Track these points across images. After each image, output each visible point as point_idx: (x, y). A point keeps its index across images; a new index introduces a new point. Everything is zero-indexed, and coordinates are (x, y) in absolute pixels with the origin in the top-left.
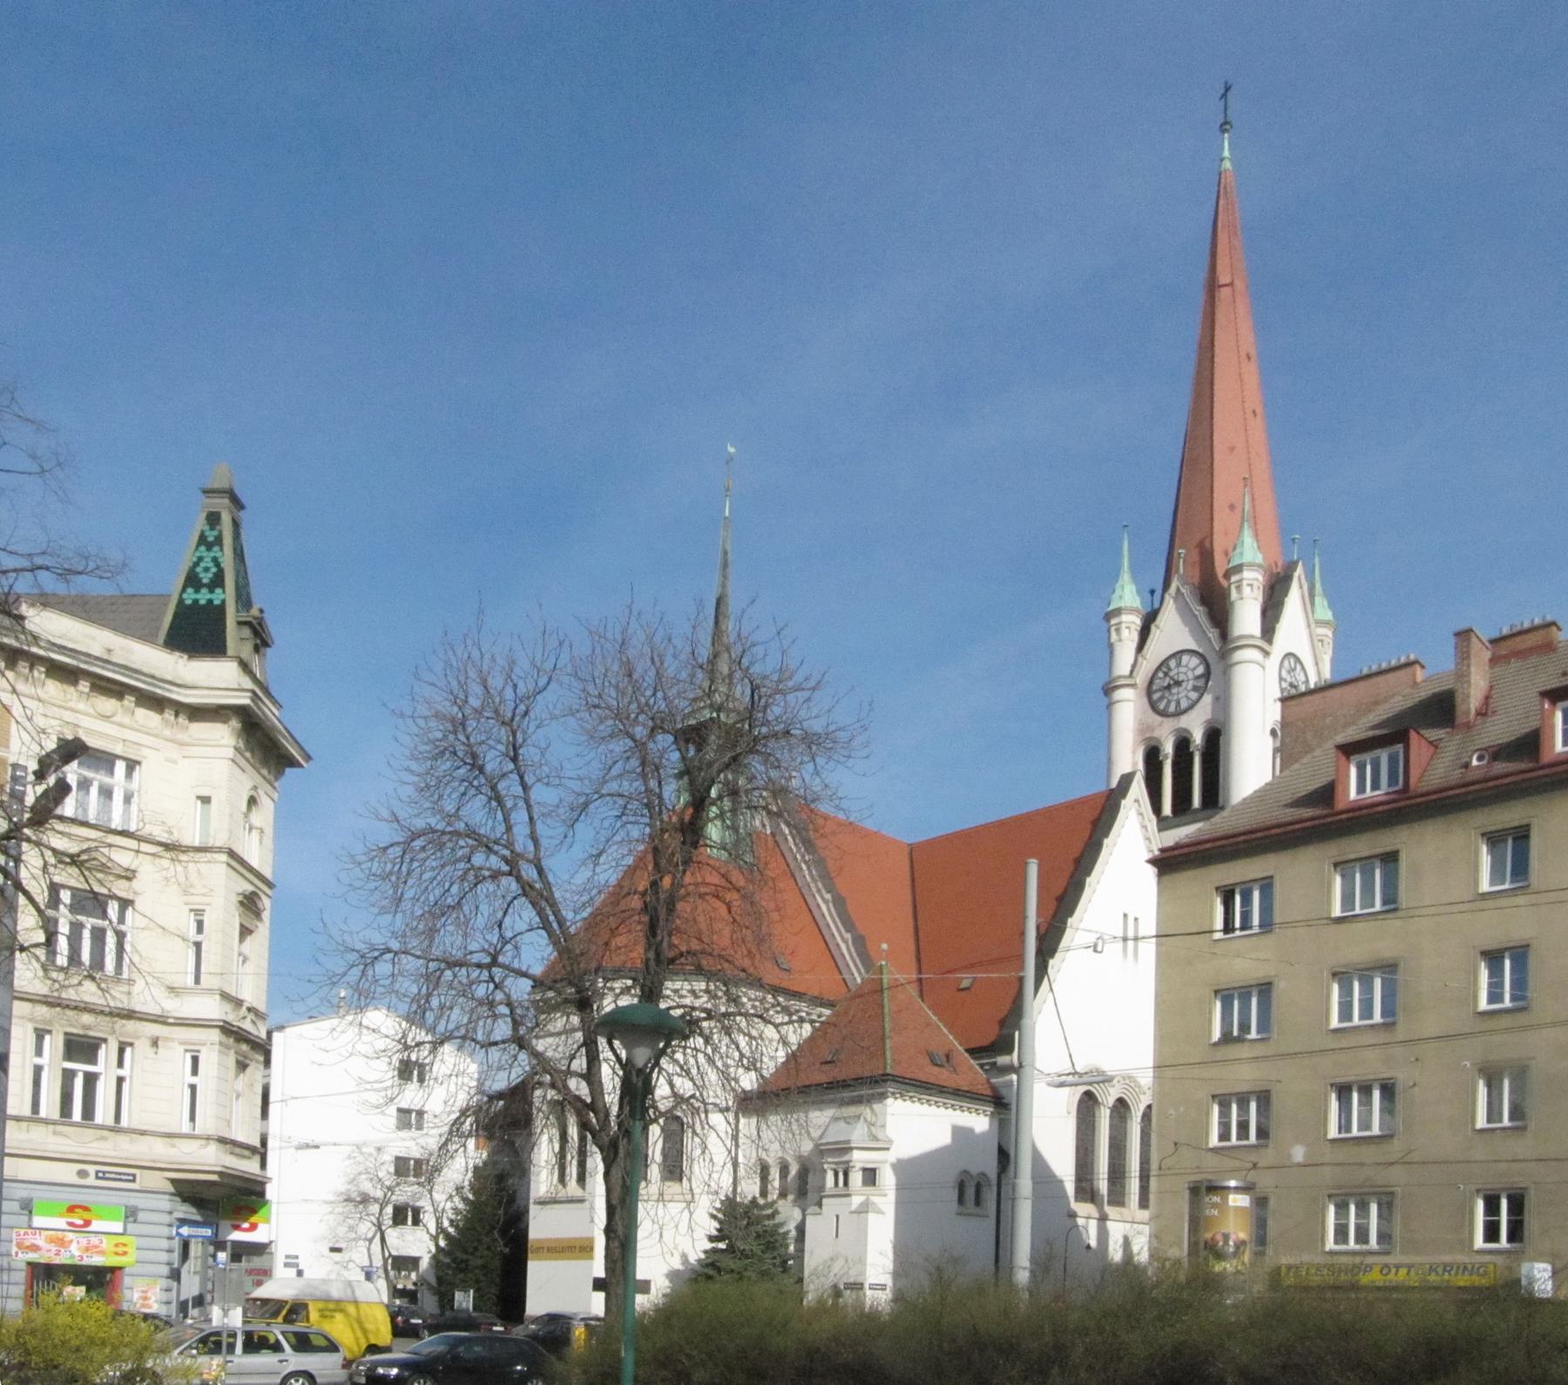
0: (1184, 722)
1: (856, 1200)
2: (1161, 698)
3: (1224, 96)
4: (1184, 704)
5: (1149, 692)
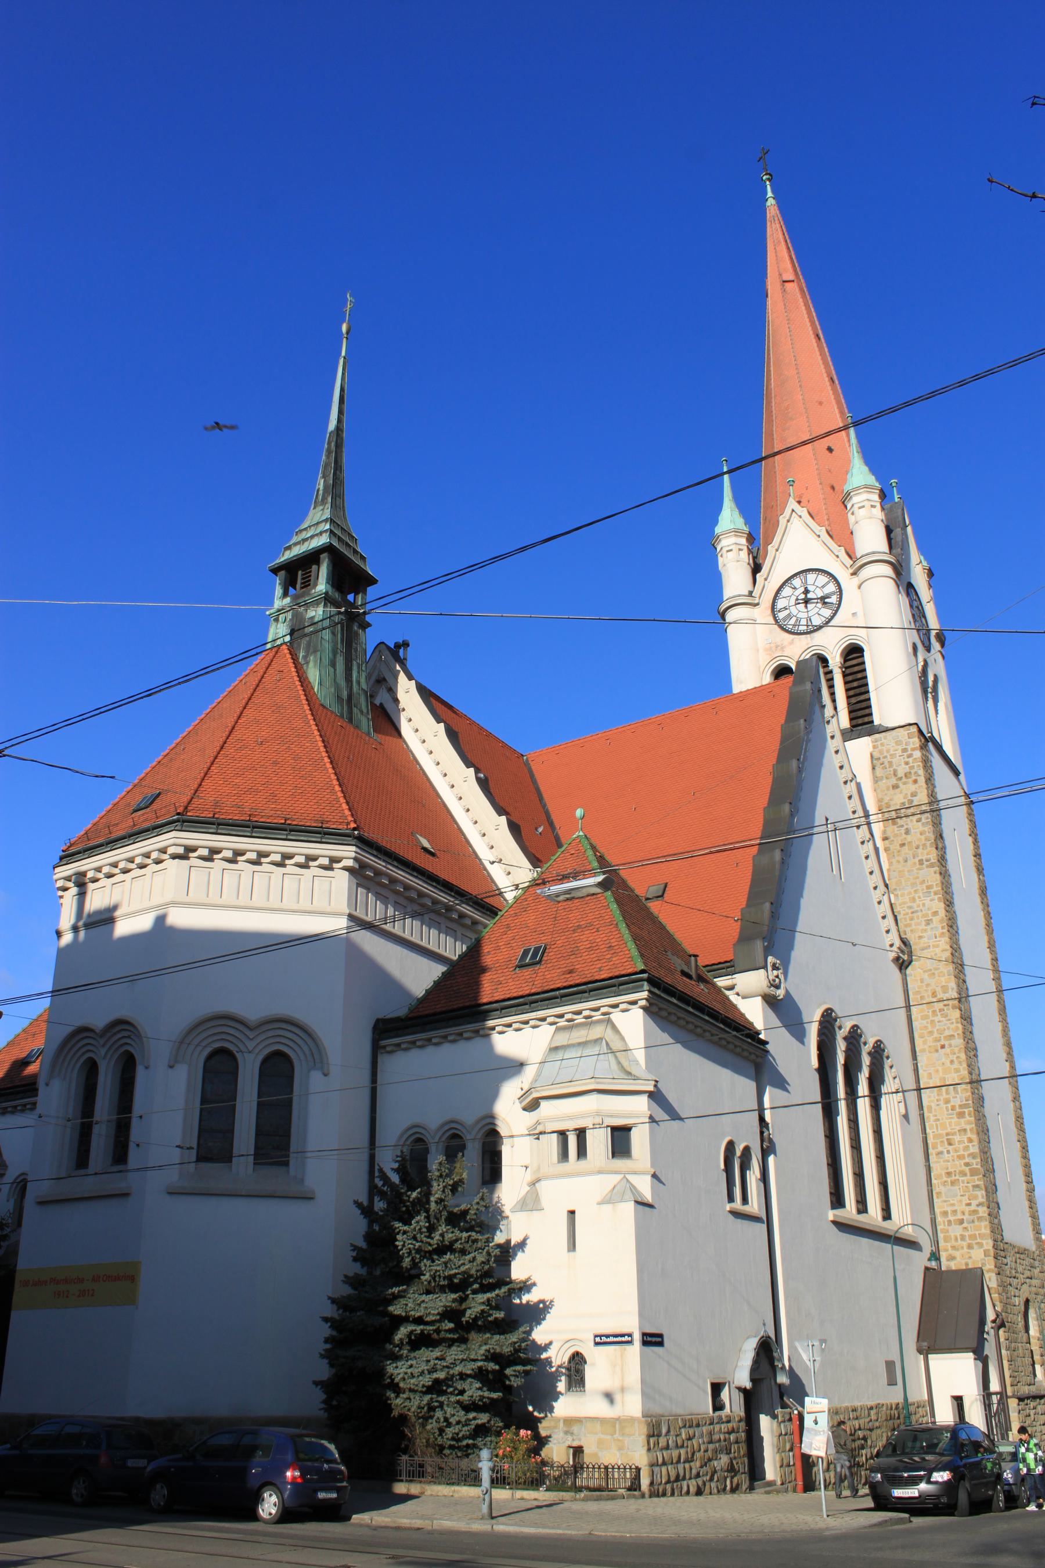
2: (789, 616)
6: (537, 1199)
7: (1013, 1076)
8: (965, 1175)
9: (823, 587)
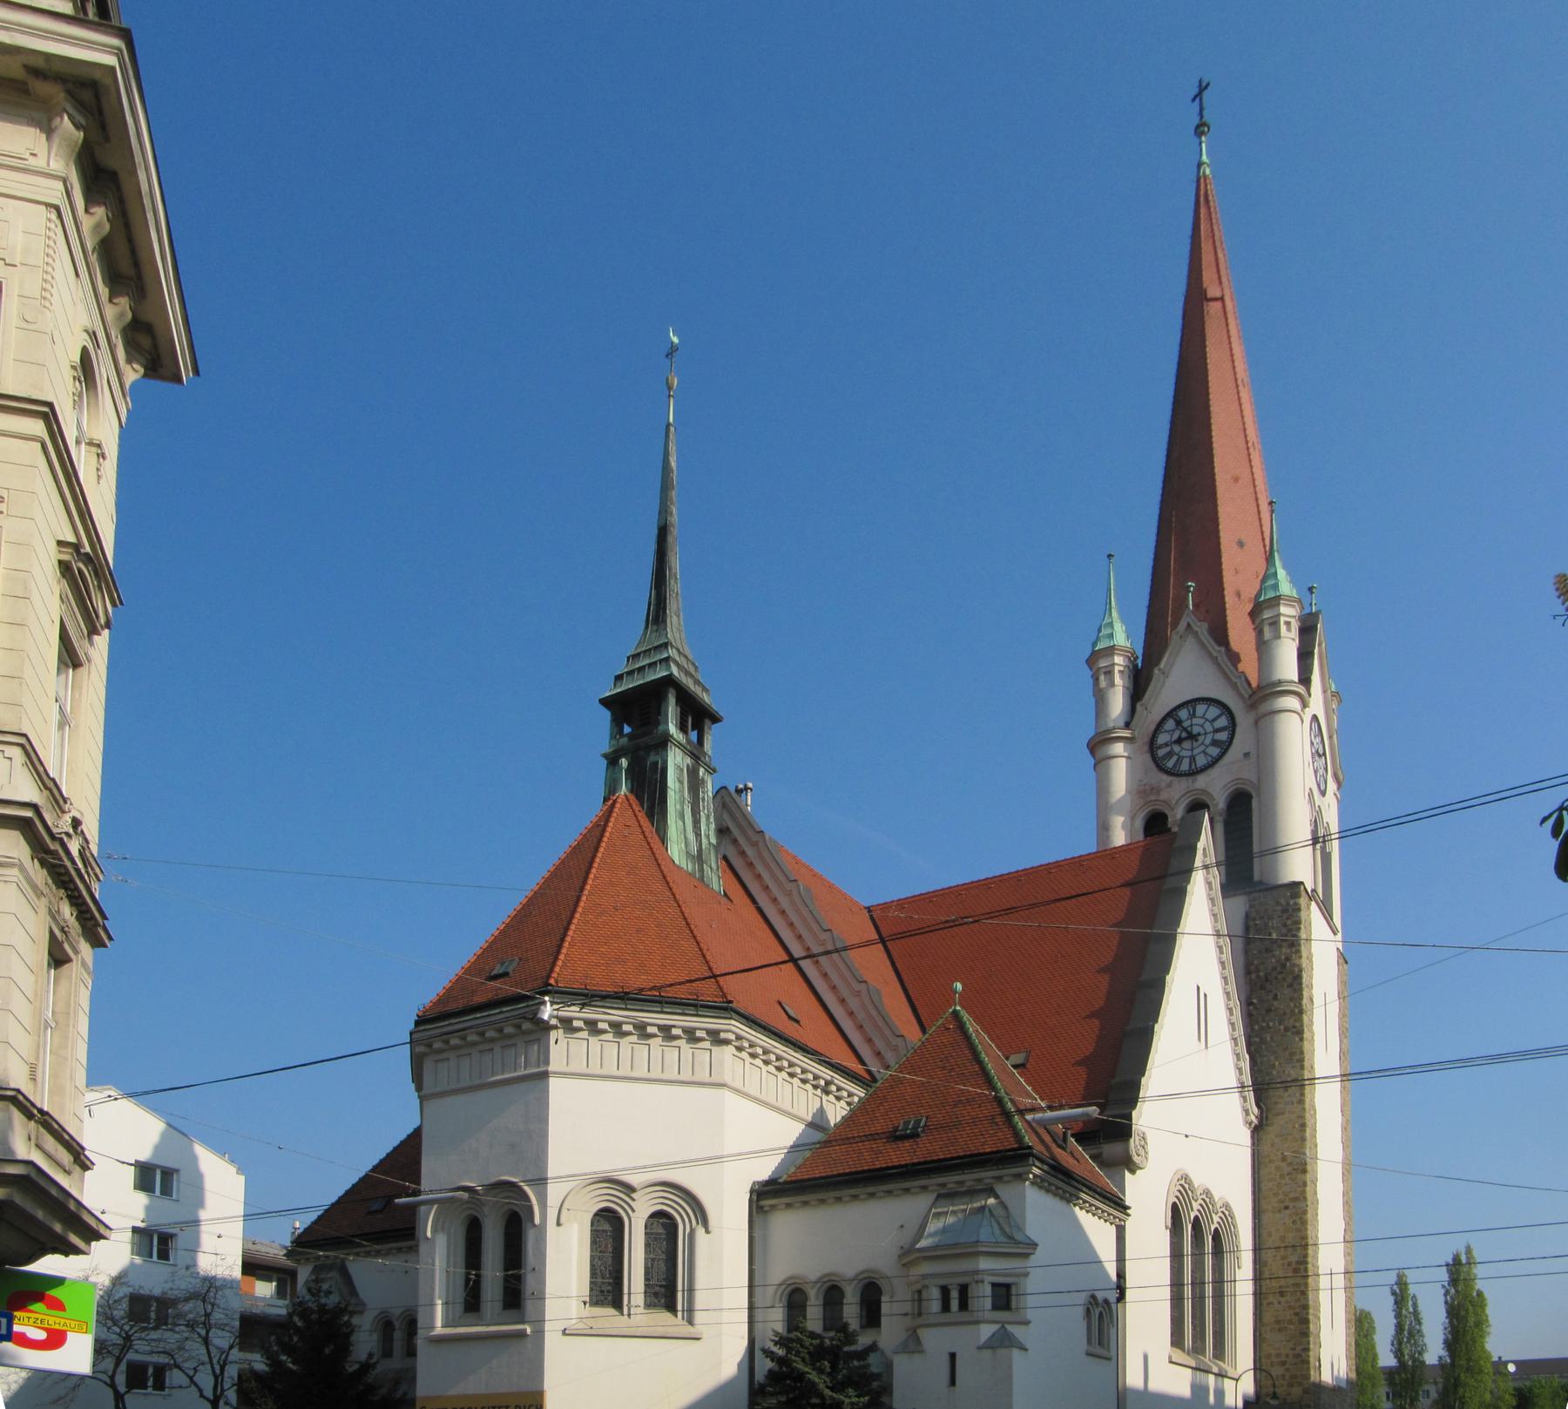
0: (1202, 781)
1: (986, 1331)
2: (1170, 754)
3: (1199, 95)
4: (1201, 761)
5: (1152, 746)
6: (918, 1341)
7: (715, 976)
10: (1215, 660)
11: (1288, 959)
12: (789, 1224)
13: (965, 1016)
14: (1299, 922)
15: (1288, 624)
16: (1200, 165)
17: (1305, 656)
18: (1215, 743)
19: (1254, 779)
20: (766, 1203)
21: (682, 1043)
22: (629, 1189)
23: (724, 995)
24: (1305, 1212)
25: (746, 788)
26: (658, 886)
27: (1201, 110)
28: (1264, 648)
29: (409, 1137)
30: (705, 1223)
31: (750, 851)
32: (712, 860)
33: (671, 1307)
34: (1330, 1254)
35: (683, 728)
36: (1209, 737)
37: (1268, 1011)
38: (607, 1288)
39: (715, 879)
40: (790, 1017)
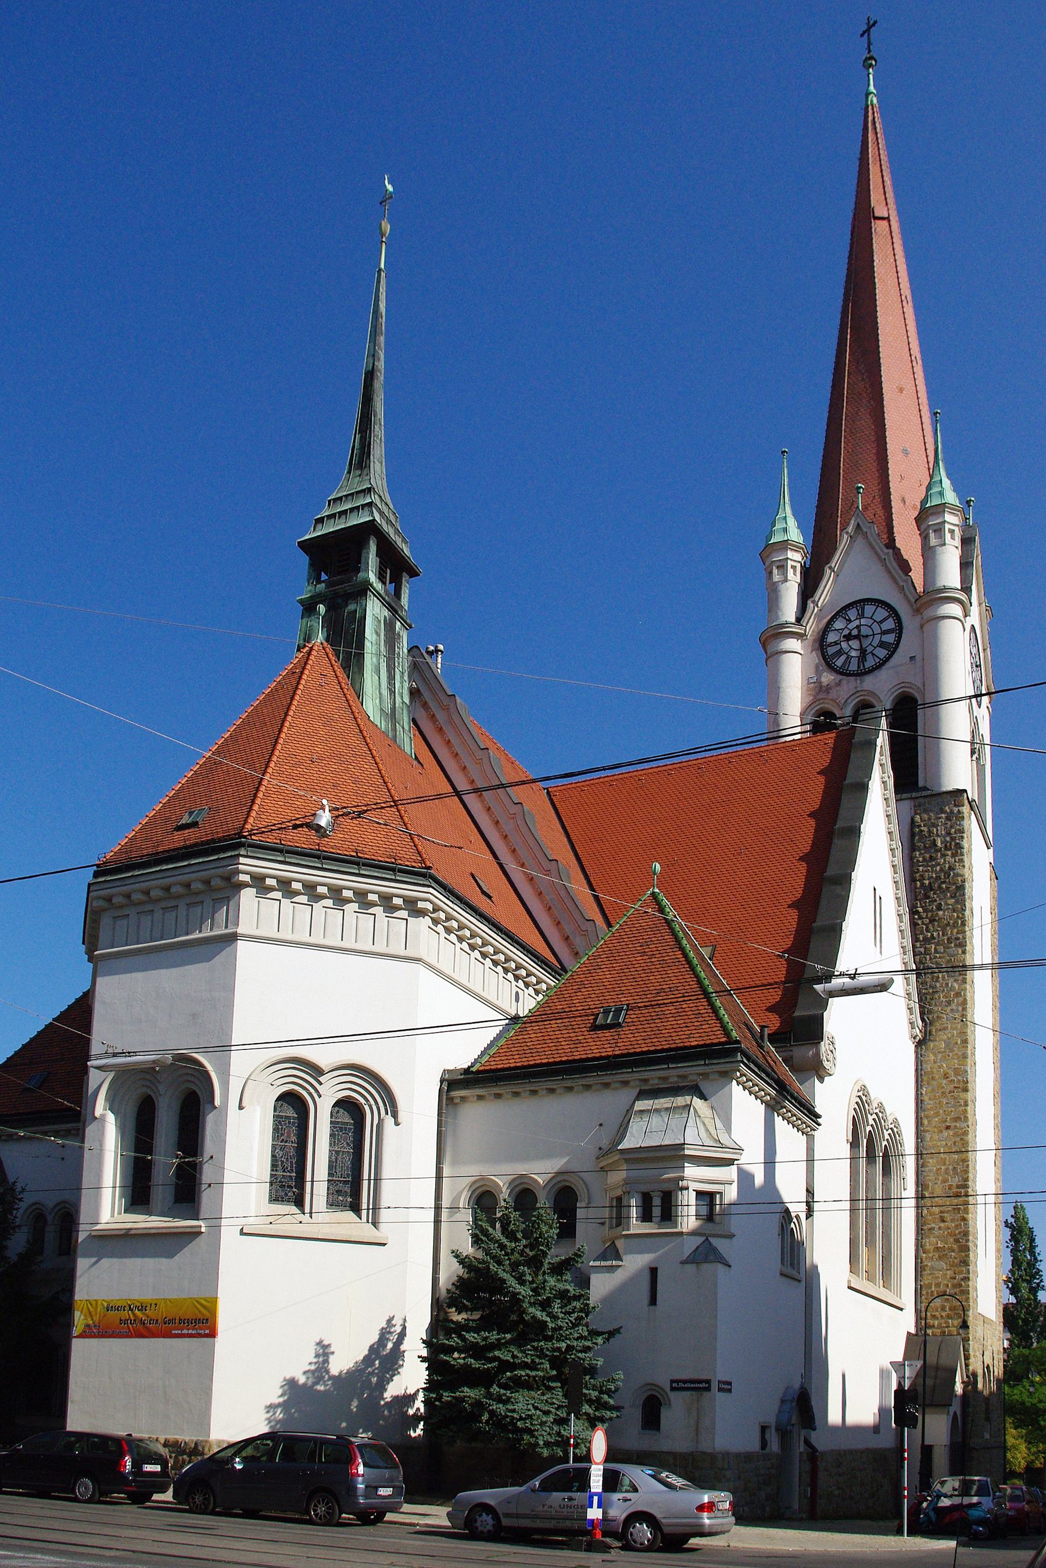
0: (869, 683)
2: (840, 653)
3: (867, 31)
8: (953, 1251)
9: (882, 622)
10: (883, 562)
11: (951, 868)
12: (478, 1114)
13: (661, 896)
14: (962, 831)
15: (952, 532)
16: (868, 94)
17: (965, 565)
18: (882, 645)
19: (919, 684)
20: (457, 1094)
21: (378, 910)
22: (316, 1071)
23: (423, 861)
24: (966, 1133)
25: (437, 651)
26: (355, 741)
27: (869, 44)
28: (928, 554)
29: (78, 1001)
30: (395, 1115)
31: (441, 716)
32: (405, 719)
33: (356, 1208)
34: (985, 1175)
35: (381, 578)
36: (877, 638)
37: (932, 921)
38: (288, 1184)
39: (407, 740)
40: (484, 893)
